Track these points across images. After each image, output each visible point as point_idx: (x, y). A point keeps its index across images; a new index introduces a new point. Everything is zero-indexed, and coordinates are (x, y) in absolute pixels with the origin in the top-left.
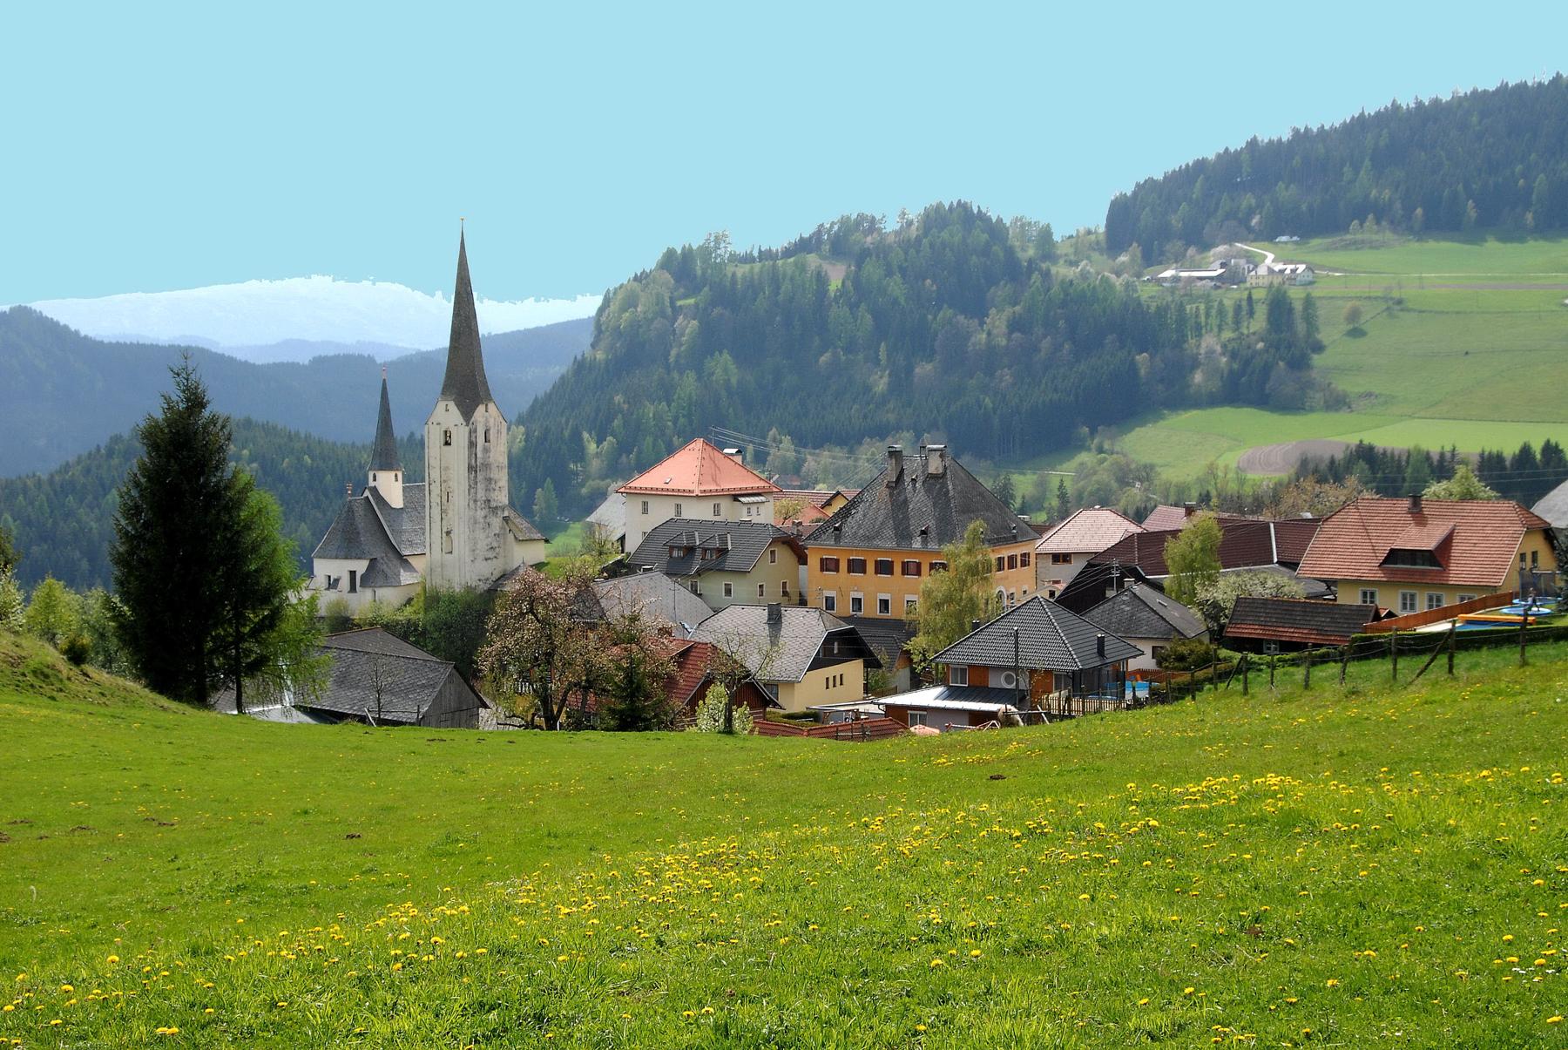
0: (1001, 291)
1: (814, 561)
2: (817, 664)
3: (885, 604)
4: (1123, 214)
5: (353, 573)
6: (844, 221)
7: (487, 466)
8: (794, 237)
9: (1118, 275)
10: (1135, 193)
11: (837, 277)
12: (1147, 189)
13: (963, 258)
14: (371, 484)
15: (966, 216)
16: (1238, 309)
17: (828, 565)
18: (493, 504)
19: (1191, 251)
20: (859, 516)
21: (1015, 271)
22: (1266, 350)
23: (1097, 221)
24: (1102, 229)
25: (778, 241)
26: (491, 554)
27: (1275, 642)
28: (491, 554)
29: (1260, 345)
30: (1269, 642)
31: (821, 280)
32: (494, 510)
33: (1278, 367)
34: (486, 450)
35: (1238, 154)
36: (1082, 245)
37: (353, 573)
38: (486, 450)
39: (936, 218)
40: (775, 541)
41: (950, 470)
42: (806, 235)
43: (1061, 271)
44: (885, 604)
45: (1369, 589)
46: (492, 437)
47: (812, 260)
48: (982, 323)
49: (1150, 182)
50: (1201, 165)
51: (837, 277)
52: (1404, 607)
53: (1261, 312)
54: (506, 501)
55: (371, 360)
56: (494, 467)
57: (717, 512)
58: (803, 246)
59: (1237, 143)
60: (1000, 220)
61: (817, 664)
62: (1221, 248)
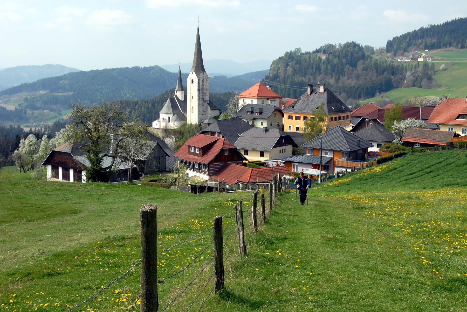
0: (360, 62)
1: (286, 116)
2: (274, 147)
3: (298, 129)
4: (390, 44)
5: (169, 118)
6: (326, 46)
7: (203, 89)
8: (315, 49)
9: (388, 58)
10: (393, 40)
11: (324, 57)
12: (396, 39)
13: (352, 55)
14: (176, 94)
15: (354, 45)
16: (416, 65)
17: (290, 118)
18: (205, 100)
19: (405, 53)
20: (299, 103)
21: (363, 57)
22: (422, 75)
23: (384, 45)
24: (385, 47)
25: (311, 50)
26: (204, 113)
27: (419, 143)
28: (204, 113)
29: (421, 74)
30: (416, 143)
31: (320, 58)
32: (205, 101)
33: (426, 78)
34: (203, 85)
35: (418, 31)
36: (381, 51)
37: (169, 118)
38: (203, 85)
39: (348, 45)
40: (275, 110)
41: (353, 103)
42: (318, 49)
43: (375, 57)
44: (298, 129)
45: (451, 127)
46: (205, 81)
47: (319, 55)
48: (356, 69)
49: (397, 37)
50: (409, 33)
51: (324, 57)
52: (463, 133)
53: (421, 67)
54: (208, 99)
55: (226, 77)
56: (205, 89)
57: (263, 102)
58: (317, 51)
59: (417, 28)
60: (362, 46)
61: (274, 147)
62: (413, 52)
